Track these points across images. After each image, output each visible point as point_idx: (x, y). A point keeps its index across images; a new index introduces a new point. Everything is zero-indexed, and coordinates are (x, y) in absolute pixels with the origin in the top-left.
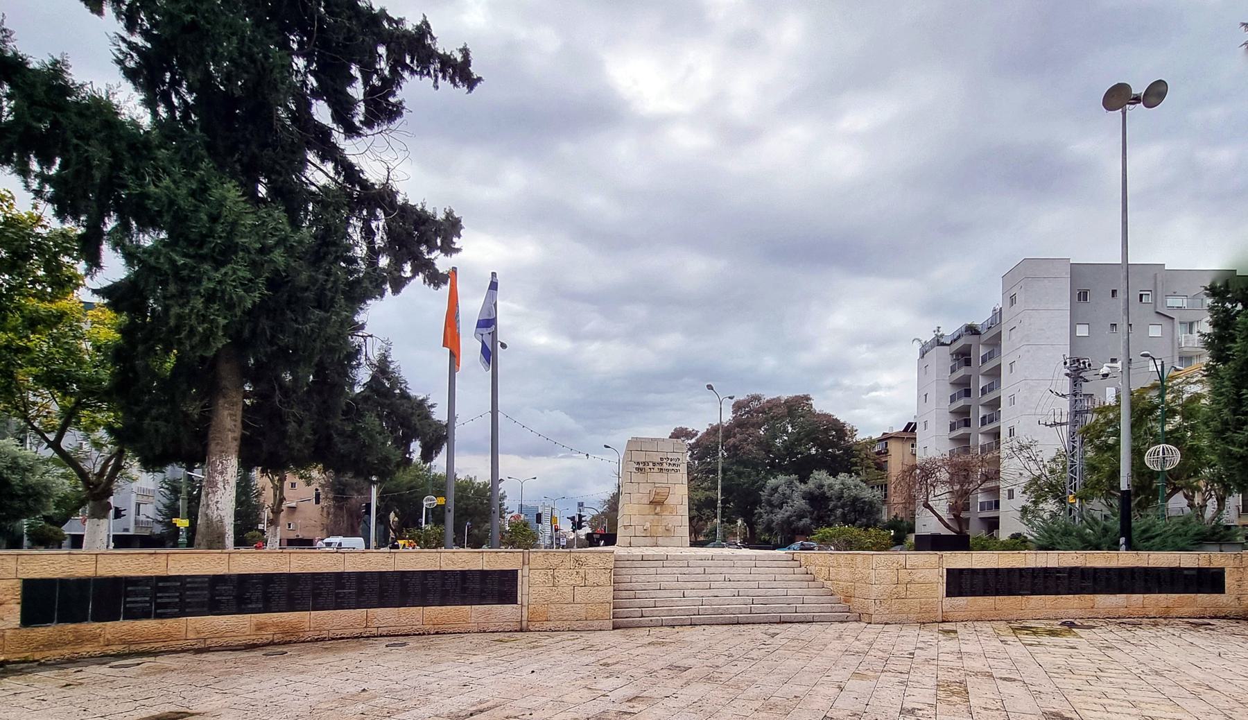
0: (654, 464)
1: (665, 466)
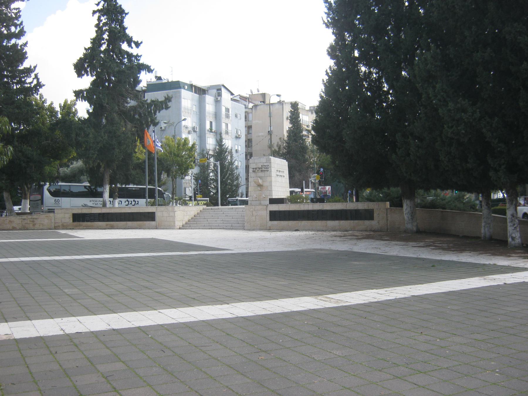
0: (259, 168)
1: (263, 169)
